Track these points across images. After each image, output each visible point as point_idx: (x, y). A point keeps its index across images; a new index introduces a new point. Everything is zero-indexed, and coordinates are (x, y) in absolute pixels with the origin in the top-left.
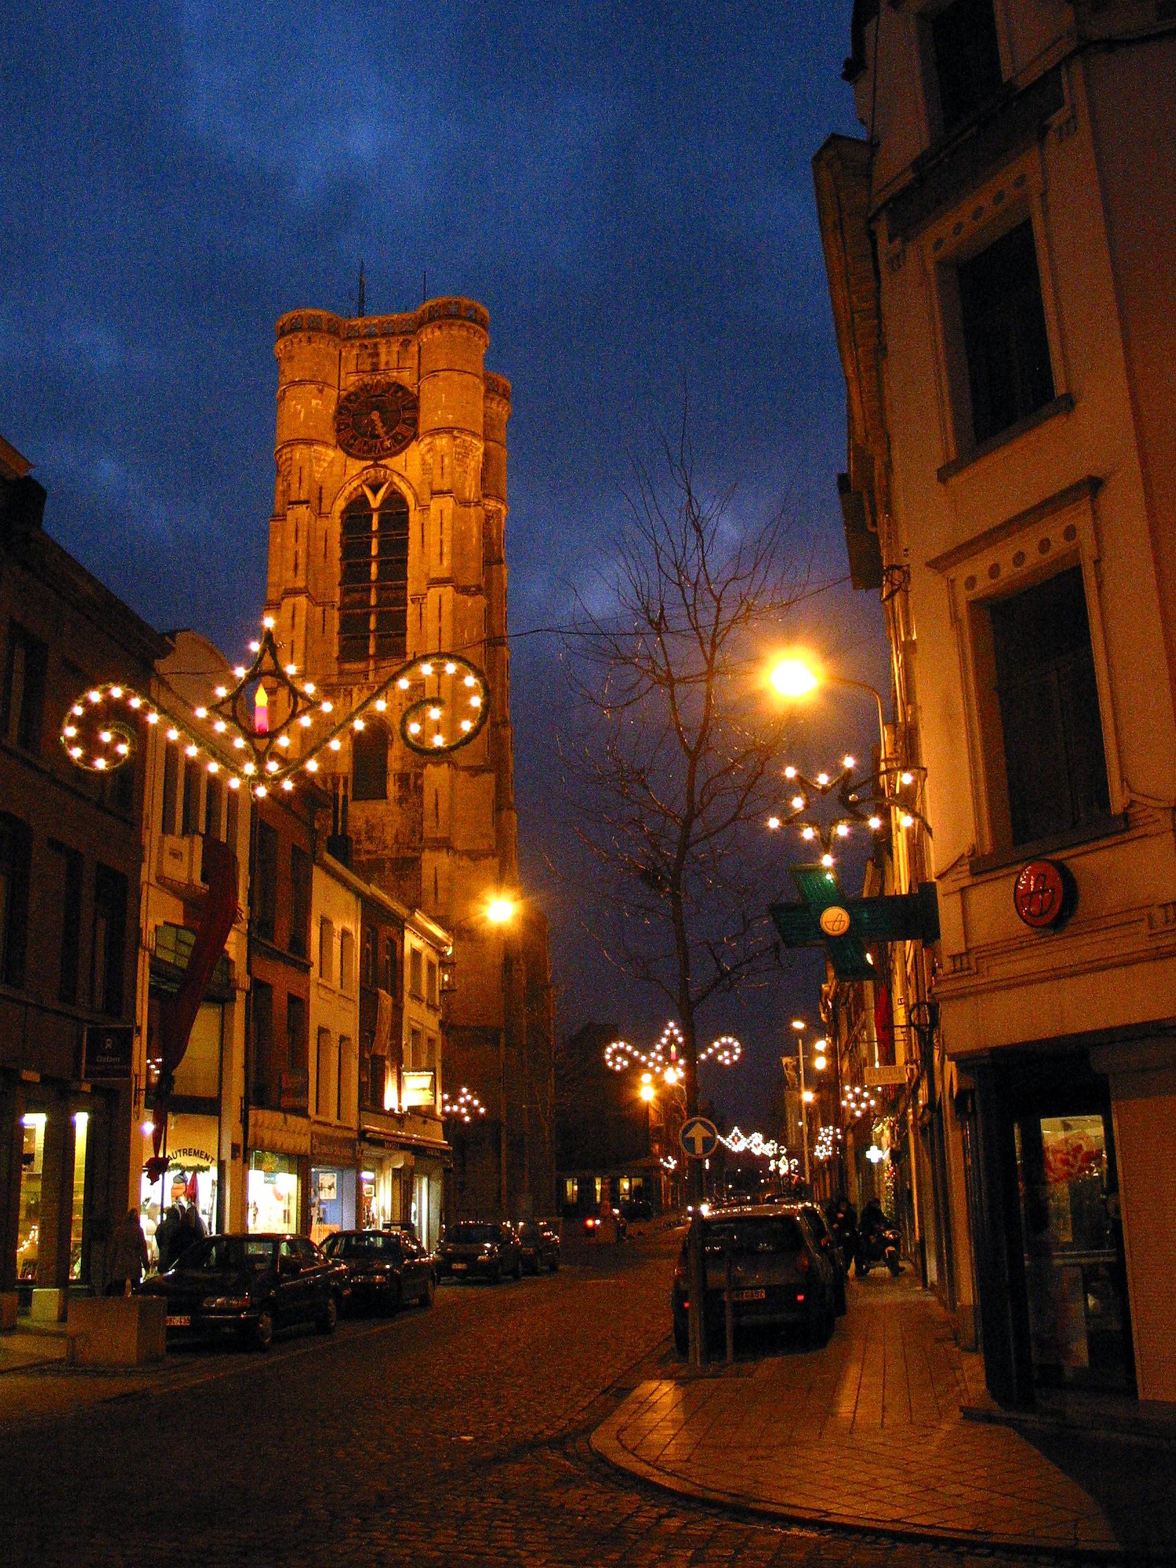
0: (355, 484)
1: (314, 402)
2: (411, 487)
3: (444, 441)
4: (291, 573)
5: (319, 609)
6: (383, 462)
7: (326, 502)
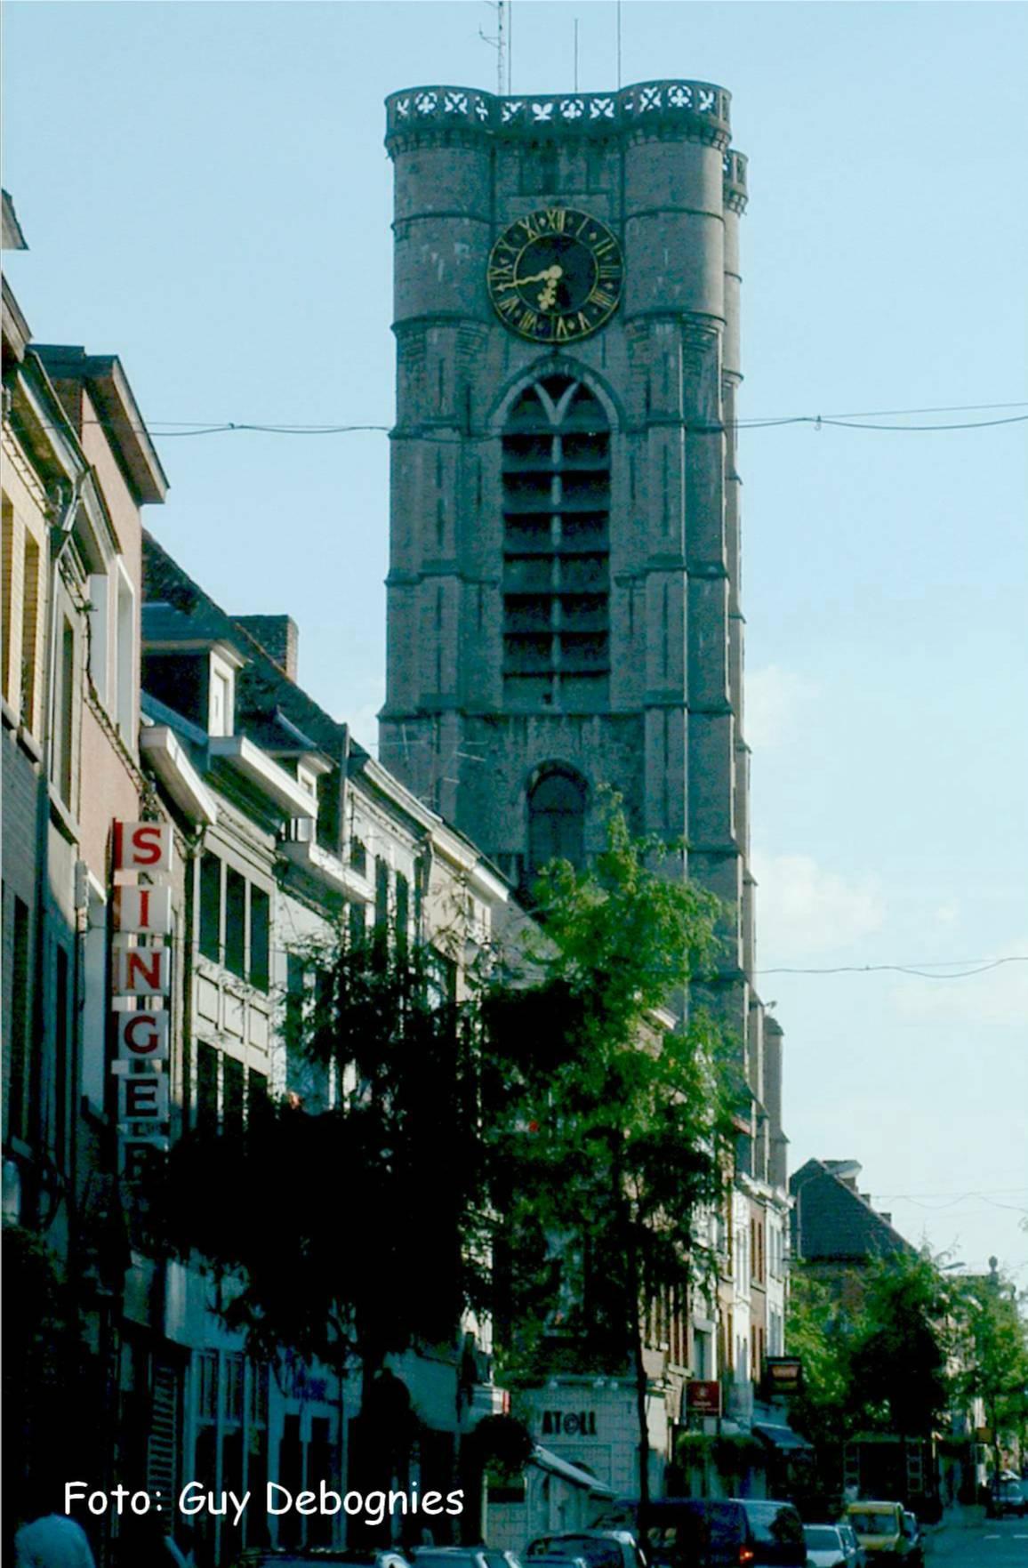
0: (523, 383)
1: (458, 247)
2: (611, 394)
3: (669, 328)
4: (433, 536)
5: (473, 588)
6: (565, 351)
7: (479, 411)
